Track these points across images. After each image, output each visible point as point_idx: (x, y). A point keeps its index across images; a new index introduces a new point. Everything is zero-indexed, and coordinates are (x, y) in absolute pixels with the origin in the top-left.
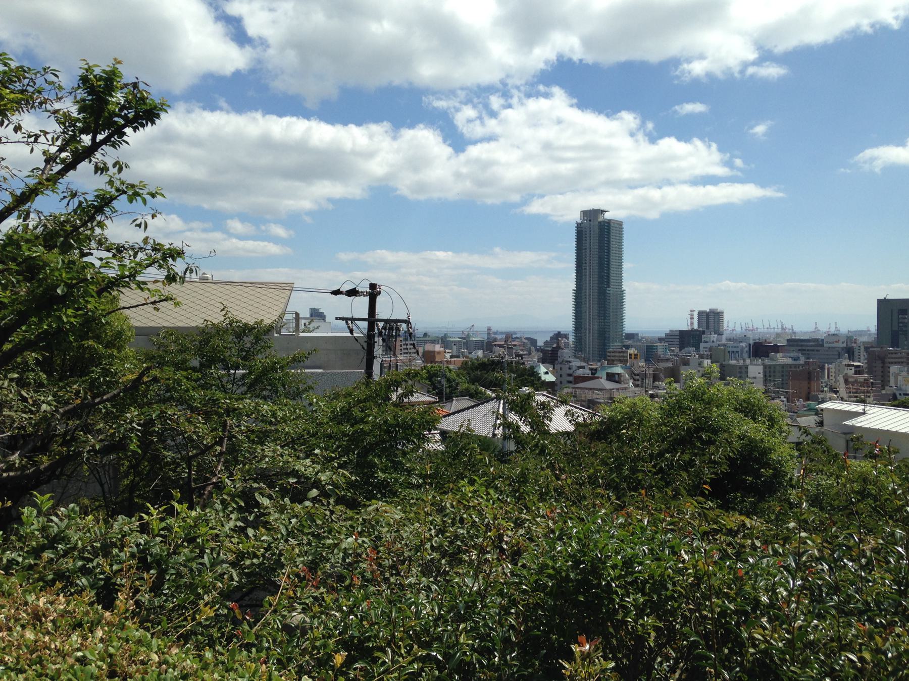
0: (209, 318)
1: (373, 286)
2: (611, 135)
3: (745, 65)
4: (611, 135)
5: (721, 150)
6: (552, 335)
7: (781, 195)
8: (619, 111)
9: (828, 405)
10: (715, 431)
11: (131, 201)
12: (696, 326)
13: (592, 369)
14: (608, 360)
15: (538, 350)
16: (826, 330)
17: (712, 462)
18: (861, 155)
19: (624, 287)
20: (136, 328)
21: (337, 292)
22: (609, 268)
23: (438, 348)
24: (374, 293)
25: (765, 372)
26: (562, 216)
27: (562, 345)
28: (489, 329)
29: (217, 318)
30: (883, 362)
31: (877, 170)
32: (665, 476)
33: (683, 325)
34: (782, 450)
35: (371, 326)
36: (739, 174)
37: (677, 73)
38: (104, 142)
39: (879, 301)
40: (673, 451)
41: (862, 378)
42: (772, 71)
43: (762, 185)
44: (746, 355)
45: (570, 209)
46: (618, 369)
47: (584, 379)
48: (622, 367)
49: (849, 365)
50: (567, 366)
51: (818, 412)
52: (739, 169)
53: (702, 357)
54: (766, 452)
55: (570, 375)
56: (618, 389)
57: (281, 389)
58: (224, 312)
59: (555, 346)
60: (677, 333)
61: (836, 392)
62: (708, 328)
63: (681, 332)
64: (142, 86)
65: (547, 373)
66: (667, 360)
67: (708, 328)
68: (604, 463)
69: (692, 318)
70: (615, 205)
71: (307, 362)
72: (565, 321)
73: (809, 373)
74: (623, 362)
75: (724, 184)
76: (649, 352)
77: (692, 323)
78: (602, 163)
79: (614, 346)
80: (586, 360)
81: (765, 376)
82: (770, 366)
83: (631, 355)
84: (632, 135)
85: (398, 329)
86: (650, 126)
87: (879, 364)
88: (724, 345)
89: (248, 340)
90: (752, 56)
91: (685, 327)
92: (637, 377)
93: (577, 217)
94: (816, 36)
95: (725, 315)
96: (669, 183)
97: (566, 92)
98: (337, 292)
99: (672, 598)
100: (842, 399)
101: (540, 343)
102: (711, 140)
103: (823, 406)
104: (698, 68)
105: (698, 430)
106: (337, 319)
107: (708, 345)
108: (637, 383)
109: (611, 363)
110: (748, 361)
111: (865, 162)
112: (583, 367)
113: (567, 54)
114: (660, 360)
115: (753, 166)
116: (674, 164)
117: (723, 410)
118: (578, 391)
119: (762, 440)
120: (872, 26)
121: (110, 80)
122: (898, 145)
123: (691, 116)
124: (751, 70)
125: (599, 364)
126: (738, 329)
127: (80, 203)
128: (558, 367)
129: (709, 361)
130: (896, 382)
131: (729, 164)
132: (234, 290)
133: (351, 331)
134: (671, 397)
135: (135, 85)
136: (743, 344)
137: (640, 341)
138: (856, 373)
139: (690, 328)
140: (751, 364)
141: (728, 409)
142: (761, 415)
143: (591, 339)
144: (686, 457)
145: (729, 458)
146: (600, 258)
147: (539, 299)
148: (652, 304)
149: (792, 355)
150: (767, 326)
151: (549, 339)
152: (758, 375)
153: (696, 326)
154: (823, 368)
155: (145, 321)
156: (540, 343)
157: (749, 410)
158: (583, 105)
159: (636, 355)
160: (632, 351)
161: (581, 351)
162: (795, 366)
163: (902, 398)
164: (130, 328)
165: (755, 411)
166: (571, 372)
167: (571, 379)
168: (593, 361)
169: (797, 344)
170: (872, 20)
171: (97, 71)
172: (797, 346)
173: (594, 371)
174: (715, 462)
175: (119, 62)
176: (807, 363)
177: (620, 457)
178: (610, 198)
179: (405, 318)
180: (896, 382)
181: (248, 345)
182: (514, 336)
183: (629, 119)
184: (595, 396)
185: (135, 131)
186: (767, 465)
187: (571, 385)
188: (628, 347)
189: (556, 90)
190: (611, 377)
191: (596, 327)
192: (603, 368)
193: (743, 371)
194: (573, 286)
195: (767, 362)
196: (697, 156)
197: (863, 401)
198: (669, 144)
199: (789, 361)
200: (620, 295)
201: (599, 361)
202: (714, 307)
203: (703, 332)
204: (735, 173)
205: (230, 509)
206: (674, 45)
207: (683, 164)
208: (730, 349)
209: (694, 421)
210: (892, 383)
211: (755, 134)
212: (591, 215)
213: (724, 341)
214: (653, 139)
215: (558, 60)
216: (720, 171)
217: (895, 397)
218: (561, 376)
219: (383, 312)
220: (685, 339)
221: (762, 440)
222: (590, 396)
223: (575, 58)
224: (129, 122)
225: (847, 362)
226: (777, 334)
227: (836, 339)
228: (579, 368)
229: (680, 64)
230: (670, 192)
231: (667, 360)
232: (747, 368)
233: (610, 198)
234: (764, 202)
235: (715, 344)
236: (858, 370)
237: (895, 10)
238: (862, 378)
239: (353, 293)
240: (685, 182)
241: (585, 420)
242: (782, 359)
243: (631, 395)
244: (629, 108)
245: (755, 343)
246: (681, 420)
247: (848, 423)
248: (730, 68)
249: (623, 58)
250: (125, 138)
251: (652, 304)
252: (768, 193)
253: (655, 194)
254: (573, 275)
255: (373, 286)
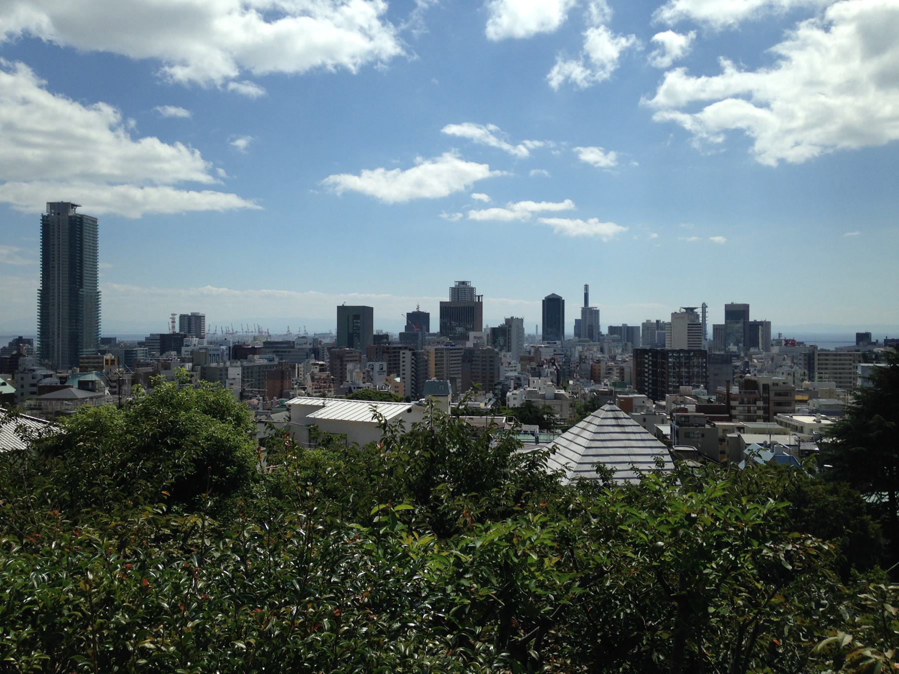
2: (88, 125)
3: (227, 80)
4: (88, 125)
5: (204, 157)
6: (11, 340)
7: (260, 208)
8: (97, 102)
9: (295, 401)
10: (183, 434)
12: (177, 330)
13: (61, 378)
14: (81, 367)
17: (175, 466)
18: (326, 179)
19: (100, 289)
22: (81, 267)
25: (243, 373)
26: (27, 206)
27: (24, 352)
30: (342, 361)
31: (339, 194)
32: (127, 486)
33: (164, 327)
34: (246, 446)
36: (222, 183)
37: (158, 75)
39: (339, 307)
40: (135, 461)
41: (324, 375)
42: (251, 90)
43: (243, 196)
44: (226, 358)
45: (37, 199)
46: (92, 377)
47: (52, 389)
48: (97, 374)
49: (315, 364)
50: (30, 375)
51: (288, 408)
52: (222, 179)
55: (33, 385)
56: (91, 398)
59: (15, 352)
61: (304, 389)
62: (189, 332)
63: (163, 337)
66: (147, 365)
67: (189, 332)
68: (57, 481)
69: (173, 322)
70: (89, 201)
73: (282, 372)
74: (98, 368)
75: (207, 192)
76: (127, 355)
77: (174, 327)
78: (78, 154)
79: (88, 351)
80: (54, 368)
81: (243, 377)
82: (248, 368)
83: (107, 361)
84: (112, 129)
86: (132, 123)
87: (338, 362)
88: (206, 349)
90: (234, 73)
91: (166, 330)
92: (114, 384)
93: (43, 210)
94: (288, 66)
95: (206, 318)
96: (152, 184)
97: (33, 70)
99: (67, 624)
100: (309, 395)
102: (195, 146)
103: (291, 402)
104: (180, 73)
105: (163, 435)
106: (586, 287)
108: (114, 390)
109: (85, 370)
110: (228, 363)
111: (330, 186)
112: (50, 376)
113: (33, 29)
115: (235, 177)
116: (157, 166)
117: (192, 413)
118: (43, 403)
119: (228, 439)
120: (336, 67)
122: (354, 175)
123: (173, 119)
124: (232, 86)
125: (70, 371)
126: (219, 333)
128: (18, 376)
130: (351, 377)
131: (212, 172)
134: (137, 404)
136: (224, 347)
138: (321, 370)
139: (171, 332)
140: (232, 366)
141: (196, 412)
142: (230, 415)
144: (150, 464)
145: (194, 460)
148: (130, 305)
151: (7, 345)
153: (177, 330)
154: (294, 367)
157: (218, 411)
158: (53, 88)
159: (113, 361)
160: (108, 356)
161: (48, 358)
162: (271, 366)
163: (355, 391)
165: (224, 411)
166: (35, 381)
167: (35, 389)
170: (335, 62)
173: (63, 380)
174: (179, 466)
176: (280, 364)
177: (76, 473)
178: (86, 192)
180: (351, 377)
183: (108, 111)
184: (64, 407)
186: (231, 463)
187: (35, 396)
188: (104, 352)
189: (21, 66)
190: (83, 385)
192: (74, 376)
193: (224, 373)
194: (36, 284)
195: (245, 363)
196: (178, 160)
197: (324, 396)
198: (152, 145)
199: (264, 362)
201: (70, 368)
202: (195, 311)
203: (185, 336)
204: (219, 182)
206: (158, 45)
207: (166, 166)
208: (212, 352)
209: (160, 427)
210: (348, 379)
211: (236, 147)
212: (60, 209)
213: (205, 345)
214: (135, 136)
215: (23, 36)
216: (204, 178)
217: (350, 390)
218: (22, 386)
220: (166, 343)
221: (228, 439)
222: (58, 407)
223: (44, 38)
225: (313, 361)
226: (255, 337)
227: (304, 340)
228: (46, 376)
229: (162, 66)
230: (153, 194)
231: (147, 365)
232: (227, 370)
233: (86, 192)
234: (244, 212)
236: (322, 369)
237: (353, 57)
238: (324, 375)
240: (167, 185)
241: (40, 435)
242: (259, 360)
243: (106, 405)
244: (110, 102)
245: (235, 346)
246: (146, 427)
248: (213, 80)
249: (101, 49)
251: (130, 305)
252: (249, 204)
253: (137, 194)
254: (38, 274)
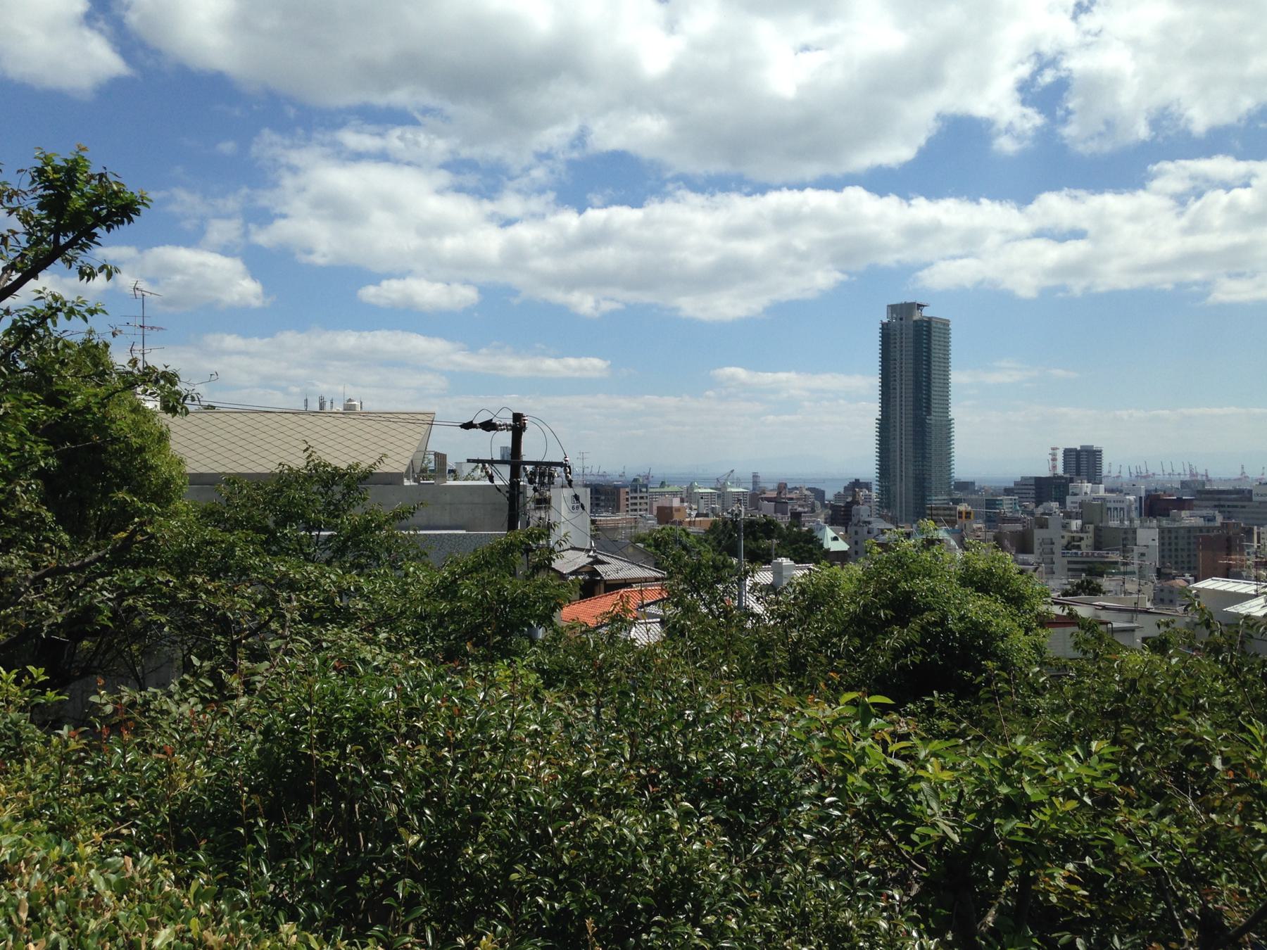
0: (284, 461)
1: (518, 417)
6: (846, 484)
11: (69, 319)
12: (1060, 471)
15: (824, 506)
16: (1258, 476)
20: (190, 474)
21: (468, 426)
23: (676, 503)
24: (518, 426)
25: (1162, 538)
28: (755, 476)
29: (298, 462)
35: (515, 474)
38: (69, 245)
44: (1134, 514)
48: (947, 531)
50: (866, 529)
53: (1068, 516)
54: (990, 638)
57: (384, 556)
58: (307, 454)
59: (850, 499)
60: (1033, 482)
63: (1039, 481)
64: (111, 178)
65: (835, 539)
66: (1017, 520)
69: (1054, 460)
71: (411, 520)
72: (866, 466)
73: (1229, 540)
77: (1054, 467)
82: (1170, 530)
83: (960, 513)
85: (551, 476)
88: (1103, 499)
89: (338, 491)
91: (1045, 472)
98: (468, 426)
101: (829, 496)
107: (1078, 499)
114: (1006, 520)
121: (71, 172)
126: (1125, 475)
127: (14, 322)
128: (852, 529)
129: (1079, 522)
132: (319, 422)
133: (491, 478)
135: (101, 176)
136: (1132, 498)
137: (976, 492)
143: (903, 489)
146: (917, 374)
147: (827, 430)
149: (1205, 512)
150: (1168, 470)
151: (842, 491)
152: (1151, 543)
153: (1060, 471)
154: (1249, 532)
155: (232, 465)
156: (829, 496)
162: (1208, 529)
164: (183, 475)
168: (907, 521)
169: (1200, 494)
171: (59, 162)
172: (1214, 500)
175: (84, 149)
179: (560, 460)
181: (338, 496)
182: (789, 486)
185: (108, 231)
188: (957, 502)
191: (911, 473)
193: (1130, 536)
195: (1165, 523)
199: (1200, 522)
200: (947, 425)
203: (1071, 480)
205: (190, 691)
208: (1109, 505)
212: (902, 311)
213: (1102, 493)
219: (532, 450)
220: (1045, 489)
224: (100, 220)
231: (1017, 520)
232: (1135, 531)
235: (1087, 498)
239: (489, 426)
242: (1189, 519)
247: (1231, 609)
250: (96, 239)
255: (518, 417)
